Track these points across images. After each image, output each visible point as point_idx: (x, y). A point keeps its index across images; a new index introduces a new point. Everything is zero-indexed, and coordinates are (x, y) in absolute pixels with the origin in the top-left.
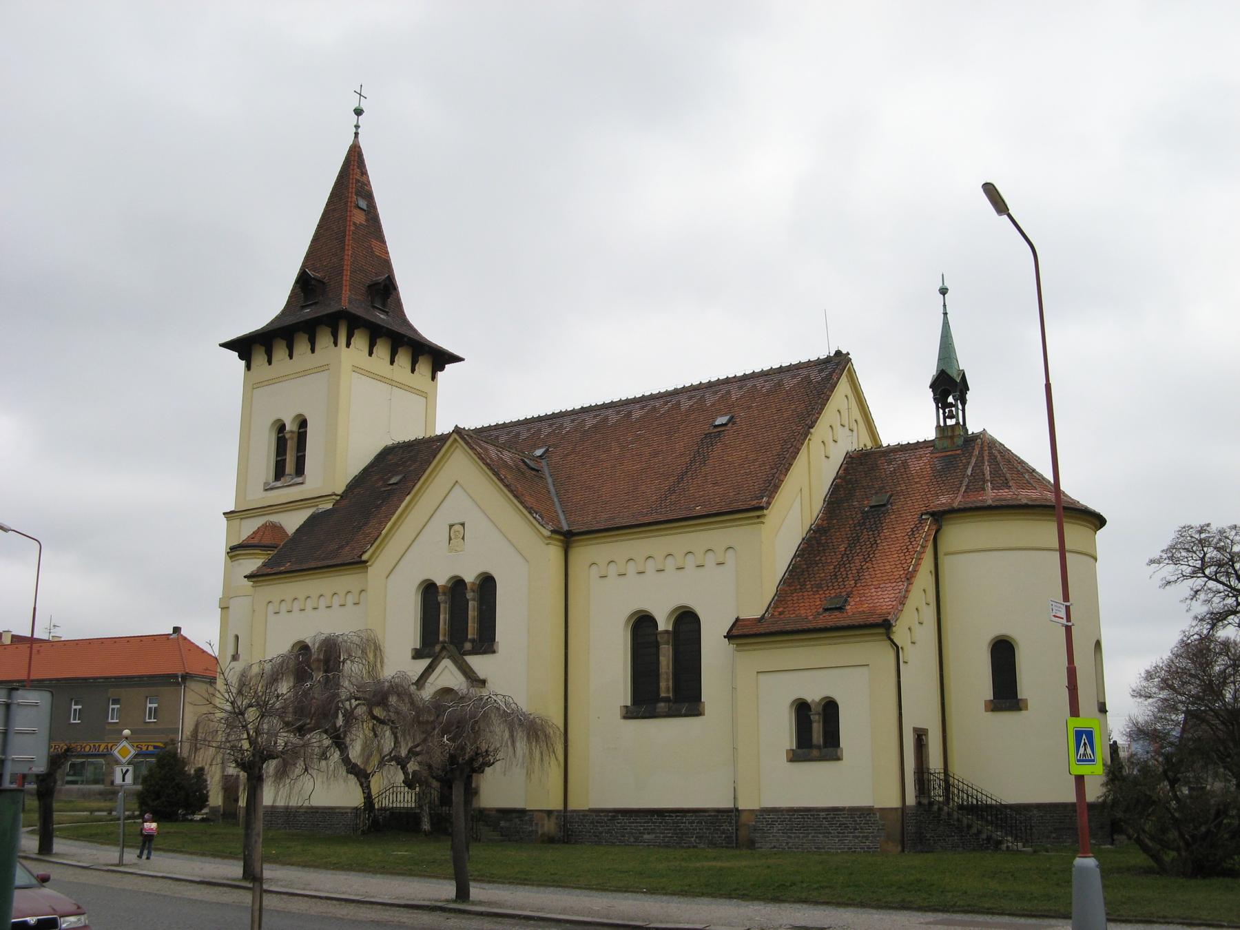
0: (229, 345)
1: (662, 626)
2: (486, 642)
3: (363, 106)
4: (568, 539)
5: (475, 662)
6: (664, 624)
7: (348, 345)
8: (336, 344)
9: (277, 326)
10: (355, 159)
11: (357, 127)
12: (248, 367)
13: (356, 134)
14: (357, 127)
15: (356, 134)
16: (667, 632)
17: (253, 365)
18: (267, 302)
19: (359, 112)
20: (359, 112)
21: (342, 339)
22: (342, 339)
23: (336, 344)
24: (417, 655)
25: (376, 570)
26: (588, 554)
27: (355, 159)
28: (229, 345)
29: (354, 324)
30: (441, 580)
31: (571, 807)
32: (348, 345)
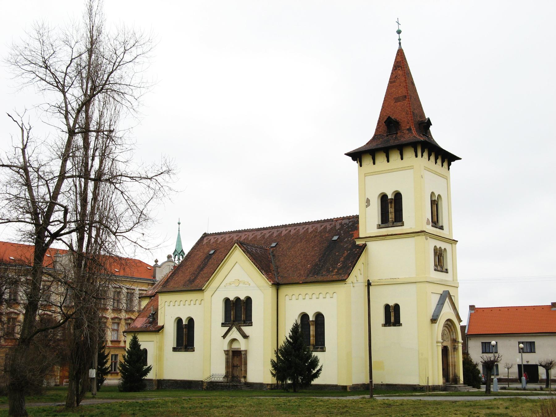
0: (348, 154)
1: (311, 319)
2: (248, 321)
3: (400, 29)
4: (277, 285)
5: (246, 329)
6: (311, 318)
7: (422, 156)
8: (416, 156)
9: (368, 148)
11: (400, 40)
12: (361, 166)
13: (400, 43)
14: (400, 40)
15: (400, 43)
16: (312, 321)
17: (363, 164)
18: (364, 133)
19: (399, 32)
20: (399, 32)
21: (419, 154)
22: (419, 154)
23: (416, 156)
24: (223, 325)
25: (207, 294)
26: (287, 292)
28: (348, 154)
29: (414, 145)
30: (232, 298)
31: (374, 382)
32: (422, 156)
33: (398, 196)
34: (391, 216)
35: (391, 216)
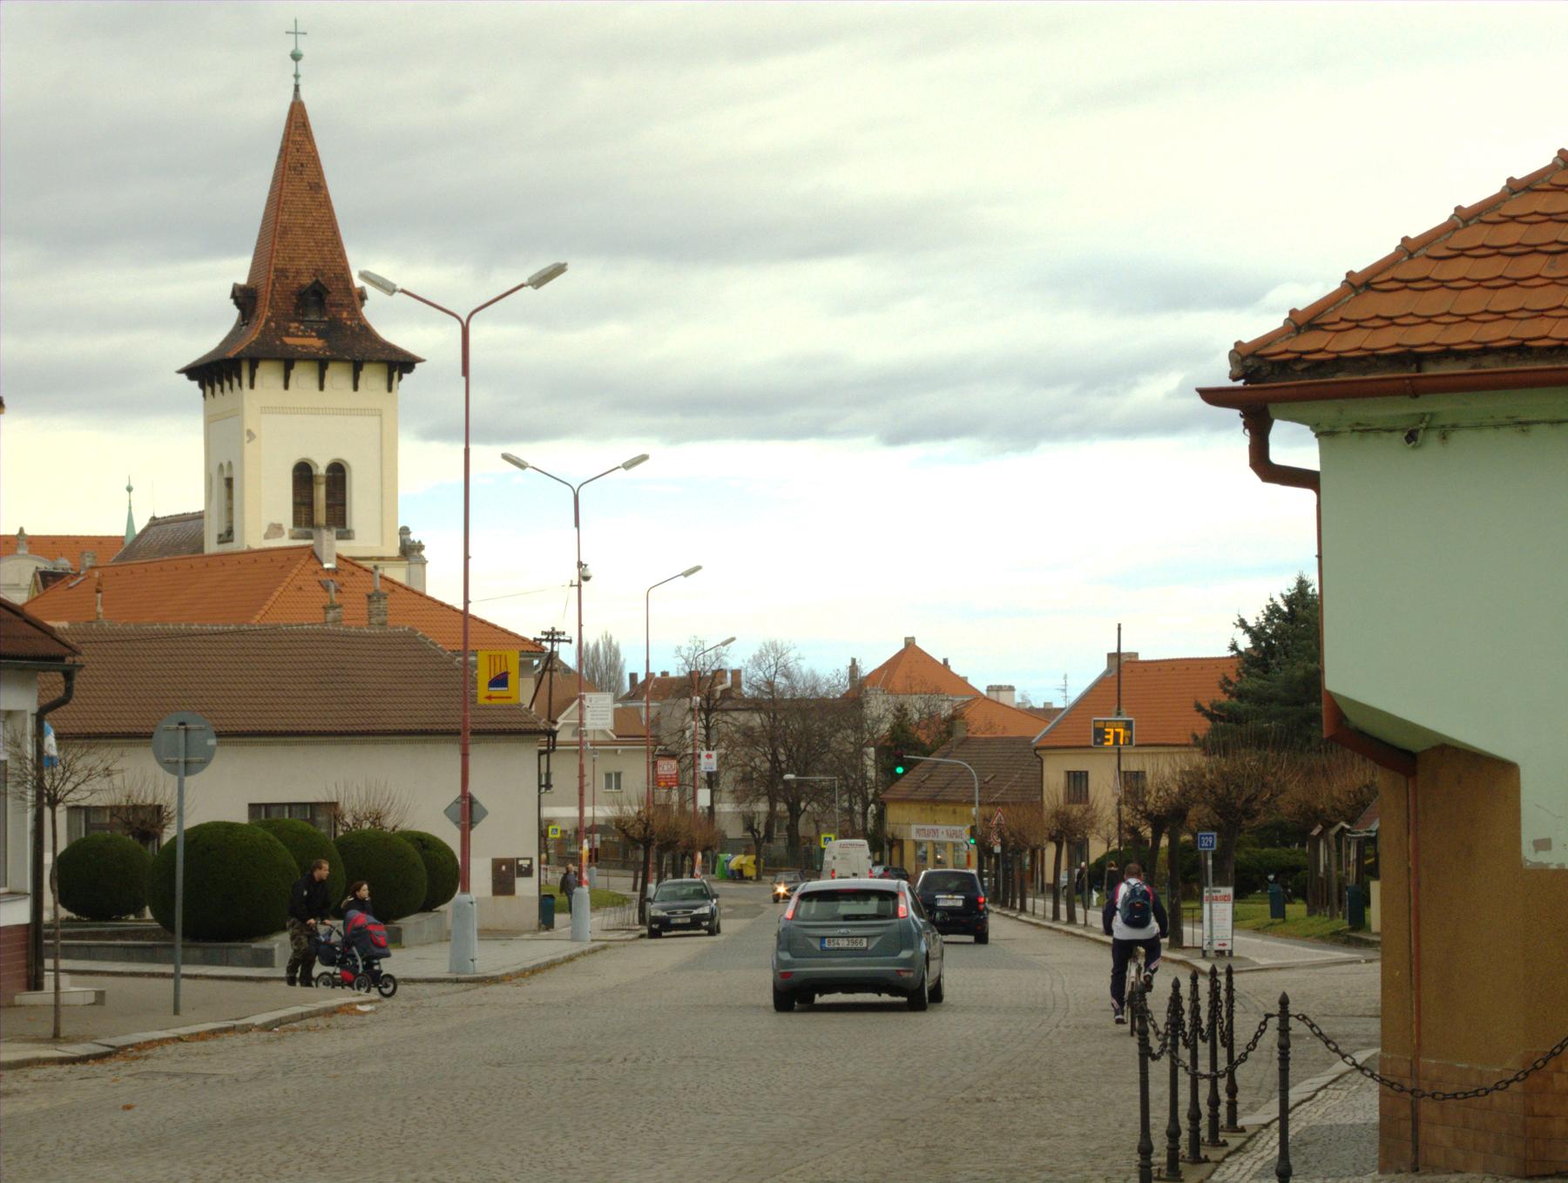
10: (298, 121)
13: (297, 88)
15: (297, 88)
20: (296, 57)
27: (298, 121)
32: (252, 386)
33: (338, 472)
34: (321, 515)
35: (321, 515)
